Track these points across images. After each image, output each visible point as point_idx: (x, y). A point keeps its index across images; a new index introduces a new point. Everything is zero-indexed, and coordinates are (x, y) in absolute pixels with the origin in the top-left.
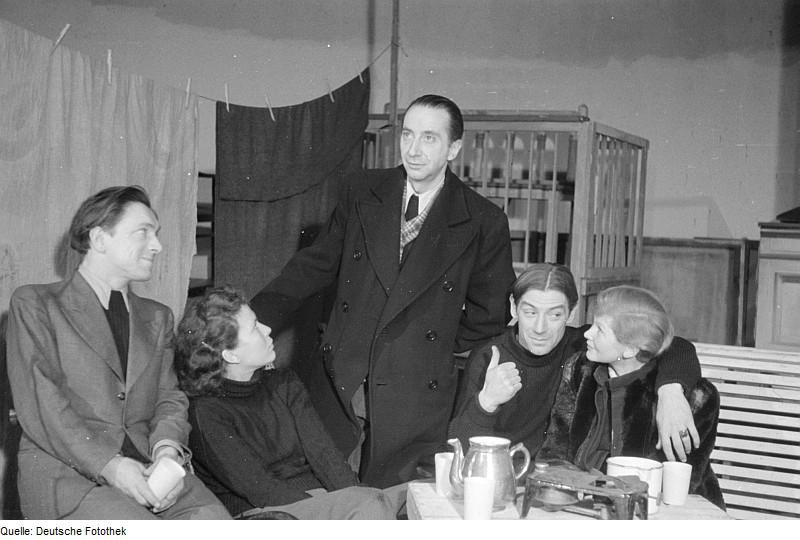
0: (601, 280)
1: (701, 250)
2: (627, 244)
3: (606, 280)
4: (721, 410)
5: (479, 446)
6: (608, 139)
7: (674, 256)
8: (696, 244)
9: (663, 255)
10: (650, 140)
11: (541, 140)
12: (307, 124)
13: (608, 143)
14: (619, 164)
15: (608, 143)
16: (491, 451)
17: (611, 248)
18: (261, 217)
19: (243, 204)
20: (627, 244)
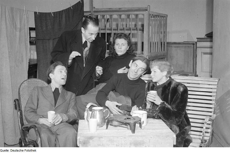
0: (153, 56)
1: (185, 45)
2: (161, 44)
3: (155, 56)
4: (188, 95)
5: (94, 110)
6: (151, 15)
7: (178, 47)
8: (184, 43)
9: (175, 47)
10: (168, 15)
11: (120, 15)
12: (64, 16)
13: (151, 16)
14: (158, 22)
15: (151, 16)
16: (98, 111)
17: (156, 47)
18: (51, 44)
19: (45, 41)
20: (161, 44)
